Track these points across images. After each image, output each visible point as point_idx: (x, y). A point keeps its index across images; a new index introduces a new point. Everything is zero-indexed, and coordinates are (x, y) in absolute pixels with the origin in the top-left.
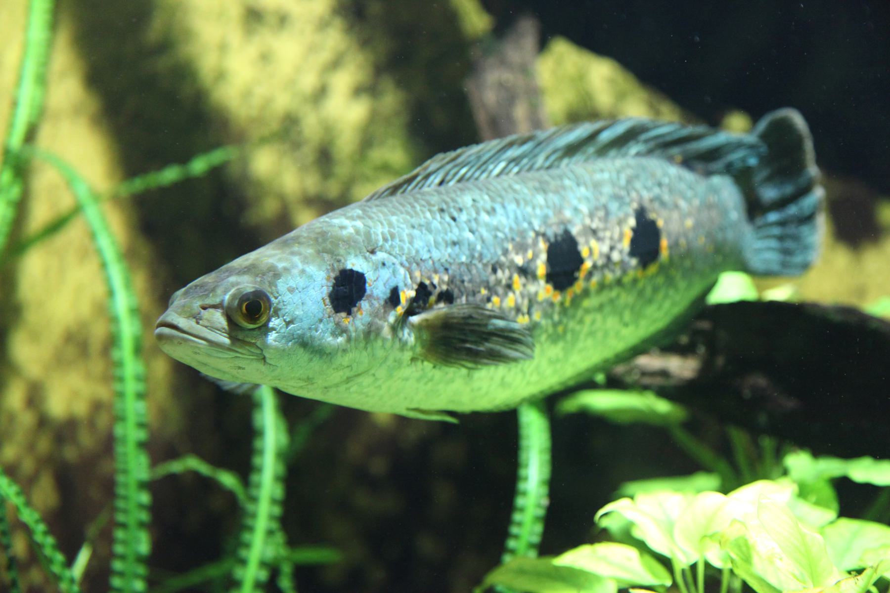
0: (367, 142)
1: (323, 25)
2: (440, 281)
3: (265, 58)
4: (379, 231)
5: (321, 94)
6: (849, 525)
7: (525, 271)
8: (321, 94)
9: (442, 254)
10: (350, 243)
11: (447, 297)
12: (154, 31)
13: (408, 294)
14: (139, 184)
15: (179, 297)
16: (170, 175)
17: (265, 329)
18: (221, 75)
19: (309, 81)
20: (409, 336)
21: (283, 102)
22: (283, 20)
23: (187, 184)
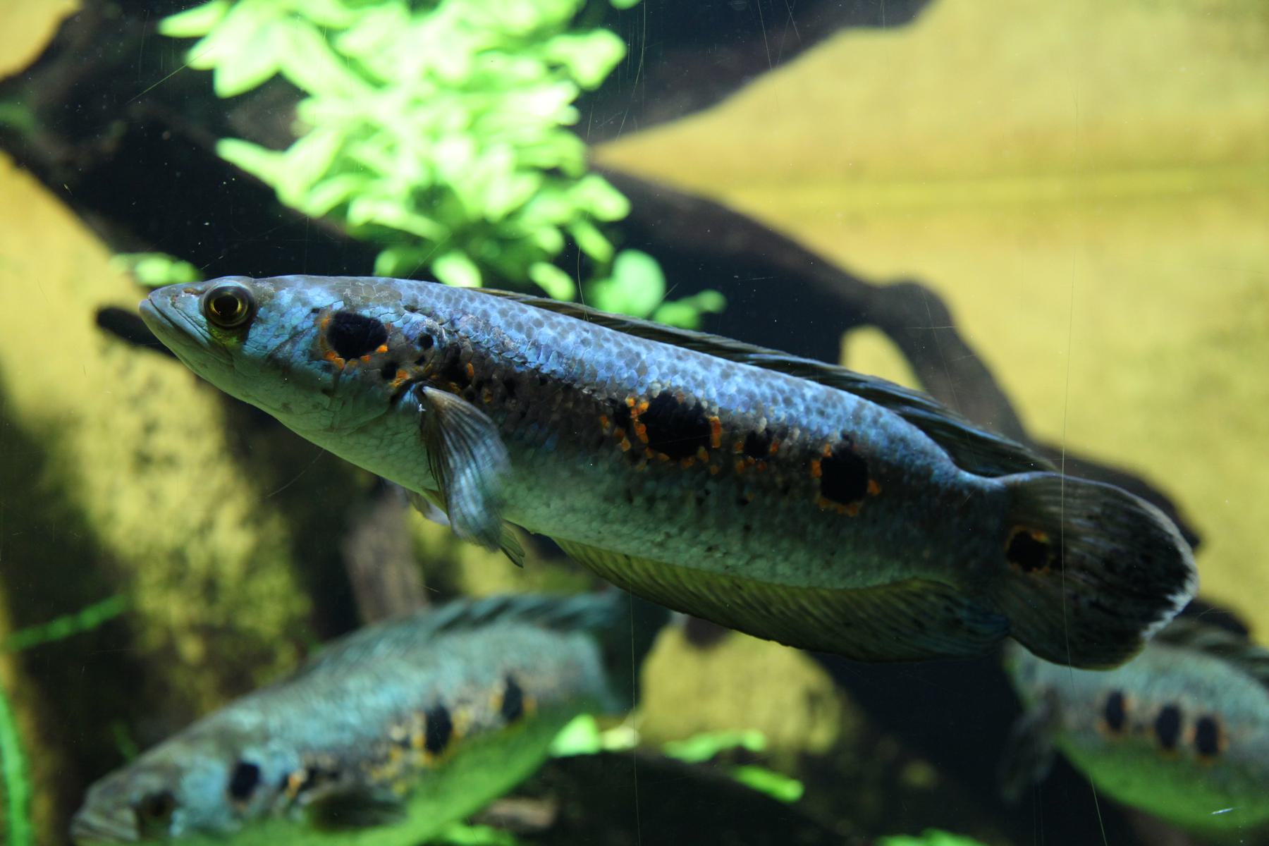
0: (252, 566)
1: (206, 463)
2: (327, 762)
3: (154, 499)
4: (274, 722)
5: (206, 528)
6: (1201, 515)
7: (405, 744)
8: (206, 528)
9: (328, 738)
10: (247, 738)
11: (334, 775)
12: (46, 481)
13: (298, 777)
14: (30, 637)
15: (95, 795)
16: (61, 628)
17: (168, 823)
18: (110, 517)
19: (195, 516)
20: (300, 815)
21: (169, 536)
22: (170, 461)
23: (77, 639)
